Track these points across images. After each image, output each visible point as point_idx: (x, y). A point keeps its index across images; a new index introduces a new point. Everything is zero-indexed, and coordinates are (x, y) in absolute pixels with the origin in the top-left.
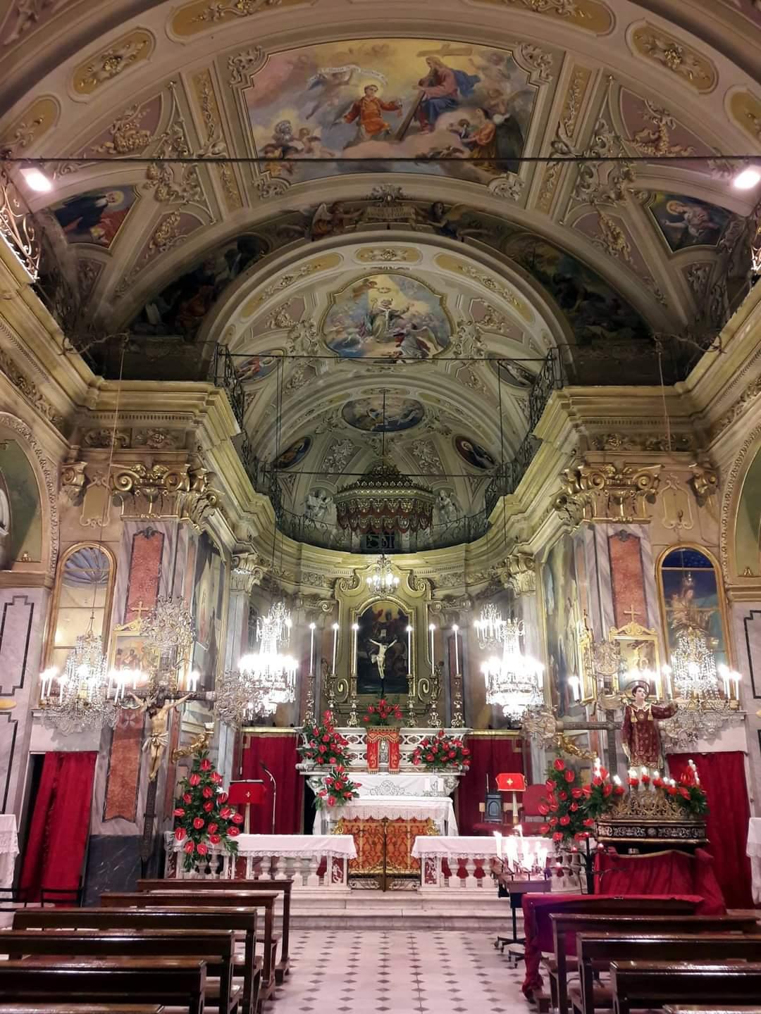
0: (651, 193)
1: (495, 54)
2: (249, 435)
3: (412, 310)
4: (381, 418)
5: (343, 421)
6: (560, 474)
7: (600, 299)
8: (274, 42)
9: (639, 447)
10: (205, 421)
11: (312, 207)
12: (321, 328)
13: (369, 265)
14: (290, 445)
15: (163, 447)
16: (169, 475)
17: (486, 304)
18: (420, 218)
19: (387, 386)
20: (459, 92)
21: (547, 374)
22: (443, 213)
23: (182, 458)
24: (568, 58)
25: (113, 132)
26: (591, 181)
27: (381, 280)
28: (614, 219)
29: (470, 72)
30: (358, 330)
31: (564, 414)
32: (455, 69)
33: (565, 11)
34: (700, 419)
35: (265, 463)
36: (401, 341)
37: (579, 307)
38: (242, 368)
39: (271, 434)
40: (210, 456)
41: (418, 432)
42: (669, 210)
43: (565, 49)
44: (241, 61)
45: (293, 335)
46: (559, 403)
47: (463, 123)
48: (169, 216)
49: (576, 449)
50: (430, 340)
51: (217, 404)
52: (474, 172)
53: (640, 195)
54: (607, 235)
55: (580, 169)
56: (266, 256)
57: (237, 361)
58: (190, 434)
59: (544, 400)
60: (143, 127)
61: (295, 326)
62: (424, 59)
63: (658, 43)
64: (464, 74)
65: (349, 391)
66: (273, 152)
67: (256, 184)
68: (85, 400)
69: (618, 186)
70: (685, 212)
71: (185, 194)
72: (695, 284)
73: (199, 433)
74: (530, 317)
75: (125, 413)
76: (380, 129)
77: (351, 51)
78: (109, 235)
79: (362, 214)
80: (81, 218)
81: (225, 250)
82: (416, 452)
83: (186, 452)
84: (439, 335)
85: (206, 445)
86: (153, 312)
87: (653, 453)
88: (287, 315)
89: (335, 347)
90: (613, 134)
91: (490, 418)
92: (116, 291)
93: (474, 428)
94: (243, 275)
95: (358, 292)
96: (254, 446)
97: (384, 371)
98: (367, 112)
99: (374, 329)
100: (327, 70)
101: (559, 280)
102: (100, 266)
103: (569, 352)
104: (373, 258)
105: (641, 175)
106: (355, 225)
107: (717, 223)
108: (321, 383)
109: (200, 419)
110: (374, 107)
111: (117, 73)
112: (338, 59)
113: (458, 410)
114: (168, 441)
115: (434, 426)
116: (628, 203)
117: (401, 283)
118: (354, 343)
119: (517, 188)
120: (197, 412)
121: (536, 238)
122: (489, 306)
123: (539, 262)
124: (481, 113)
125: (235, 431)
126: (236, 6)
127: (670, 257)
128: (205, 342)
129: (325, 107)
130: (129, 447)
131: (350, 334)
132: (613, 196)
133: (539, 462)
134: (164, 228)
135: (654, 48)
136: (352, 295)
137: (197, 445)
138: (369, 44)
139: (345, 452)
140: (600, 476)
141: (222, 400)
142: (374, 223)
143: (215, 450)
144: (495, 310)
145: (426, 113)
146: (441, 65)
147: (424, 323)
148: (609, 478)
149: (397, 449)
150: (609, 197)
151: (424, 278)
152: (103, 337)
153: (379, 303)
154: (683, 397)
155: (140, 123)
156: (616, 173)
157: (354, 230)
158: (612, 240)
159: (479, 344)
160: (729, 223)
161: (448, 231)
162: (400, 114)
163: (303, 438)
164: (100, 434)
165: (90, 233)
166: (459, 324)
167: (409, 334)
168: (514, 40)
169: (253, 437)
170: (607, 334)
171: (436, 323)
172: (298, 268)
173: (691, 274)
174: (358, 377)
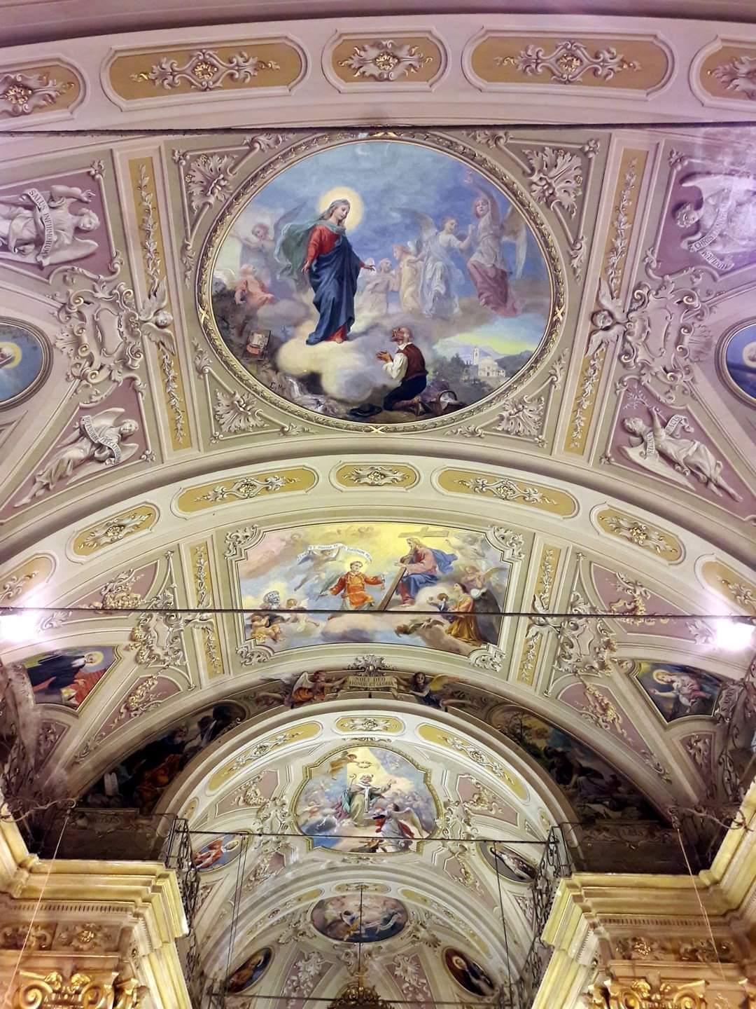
0: (635, 662)
1: (470, 536)
2: (199, 942)
3: (394, 788)
4: (357, 923)
5: (311, 926)
6: (582, 994)
7: (598, 775)
8: (269, 522)
9: (672, 956)
10: (147, 914)
11: (294, 675)
12: (294, 807)
13: (349, 735)
14: (245, 959)
15: (90, 949)
16: (90, 989)
17: (474, 781)
18: (402, 688)
19: (366, 881)
20: (437, 569)
21: (551, 858)
22: (426, 683)
23: (109, 965)
24: (537, 538)
25: (104, 593)
26: (571, 651)
27: (362, 753)
28: (599, 688)
29: (448, 552)
30: (334, 811)
31: (578, 909)
32: (434, 548)
33: (531, 499)
34: (737, 919)
35: (214, 980)
36: (382, 824)
37: (576, 783)
38: (200, 853)
39: (223, 942)
40: (146, 965)
41: (400, 943)
42: (655, 679)
43: (535, 531)
44: (238, 537)
45: (263, 814)
46: (570, 894)
47: (441, 597)
48: (146, 680)
49: (598, 959)
50: (414, 824)
51: (165, 890)
52: (454, 642)
53: (624, 664)
54: (595, 707)
55: (559, 640)
56: (242, 723)
57: (198, 842)
58: (126, 932)
59: (549, 892)
60: (133, 591)
61: (265, 803)
62: (404, 540)
63: (621, 522)
64: (442, 554)
65: (320, 886)
66: (260, 620)
67: (240, 651)
68: (10, 885)
69: (600, 655)
70: (673, 682)
71: (167, 658)
72: (697, 757)
73: (138, 931)
74: (524, 795)
75: (53, 903)
76: (363, 601)
77: (339, 531)
78: (80, 697)
79: (344, 682)
80: (53, 678)
81: (200, 717)
82: (398, 972)
83: (117, 956)
84: (424, 818)
85: (143, 949)
86: (111, 782)
87: (691, 965)
88: (258, 791)
89: (308, 831)
90: (589, 605)
91: (485, 923)
92: (76, 757)
93: (468, 938)
94: (215, 743)
95: (336, 767)
96: (202, 957)
97: (362, 862)
98: (351, 585)
99: (352, 810)
100: (317, 548)
101: (550, 753)
102: (64, 728)
103: (572, 832)
104: (353, 728)
105: (624, 644)
106: (336, 692)
107: (708, 692)
108: (289, 875)
109: (141, 911)
110: (358, 582)
111: (118, 540)
112: (327, 538)
113: (448, 913)
114: (97, 941)
115: (419, 935)
116: (613, 672)
117: (382, 757)
118: (329, 826)
119: (498, 659)
120: (139, 900)
121: (523, 710)
122: (477, 783)
123: (526, 734)
124: (459, 588)
125: (182, 930)
126: (238, 489)
127: (665, 728)
128: (162, 815)
129: (313, 581)
130: (49, 948)
131: (325, 815)
132: (596, 666)
133: (552, 980)
134: (139, 691)
135: (619, 527)
136: (330, 769)
137: (132, 948)
138: (357, 526)
139: (313, 970)
140: (633, 997)
141: (172, 886)
142: (356, 691)
143: (153, 957)
144: (484, 788)
145: (407, 586)
146: (421, 546)
147: (407, 803)
148: (644, 999)
149: (376, 967)
150: (592, 667)
151: (405, 750)
152: (48, 802)
153: (358, 779)
154: (711, 889)
155: (132, 586)
156: (596, 643)
157: (335, 698)
158: (601, 712)
159: (468, 829)
160: (721, 693)
161: (431, 701)
162: (383, 588)
163: (263, 949)
164: (17, 930)
165: (60, 693)
166: (446, 805)
167: (390, 817)
168: (485, 523)
169: (203, 945)
170: (611, 813)
171: (420, 803)
172: (274, 737)
173: (691, 747)
174: (332, 869)
